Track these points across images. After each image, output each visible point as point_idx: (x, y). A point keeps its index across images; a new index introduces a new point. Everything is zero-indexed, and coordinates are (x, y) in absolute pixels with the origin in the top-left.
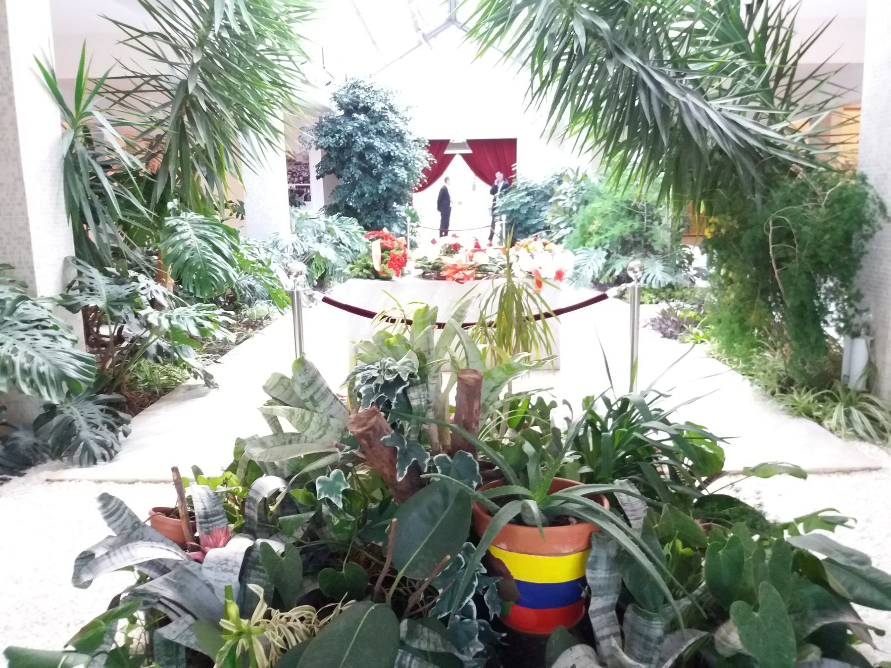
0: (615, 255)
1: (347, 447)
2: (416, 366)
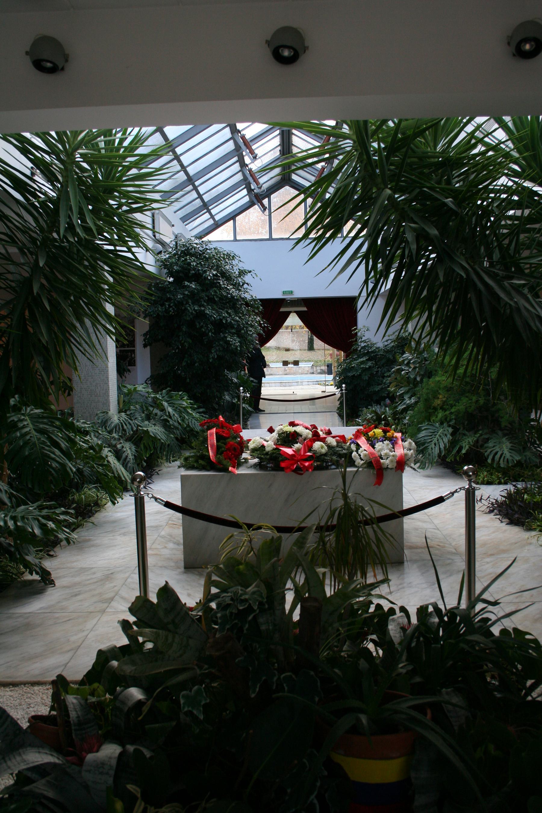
0: (461, 431)
1: (206, 666)
2: (264, 595)
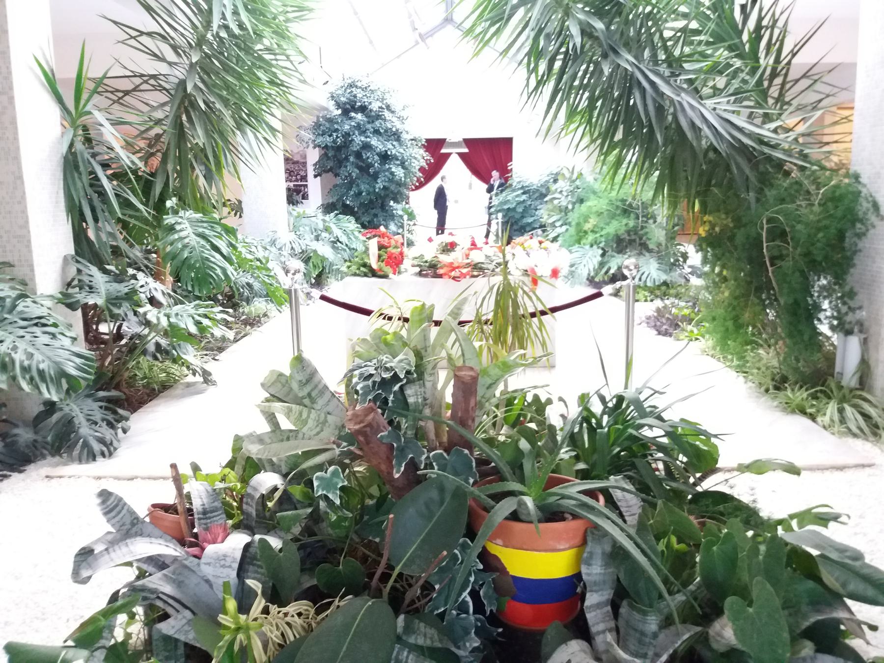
0: (610, 253)
1: (345, 444)
2: (413, 363)
